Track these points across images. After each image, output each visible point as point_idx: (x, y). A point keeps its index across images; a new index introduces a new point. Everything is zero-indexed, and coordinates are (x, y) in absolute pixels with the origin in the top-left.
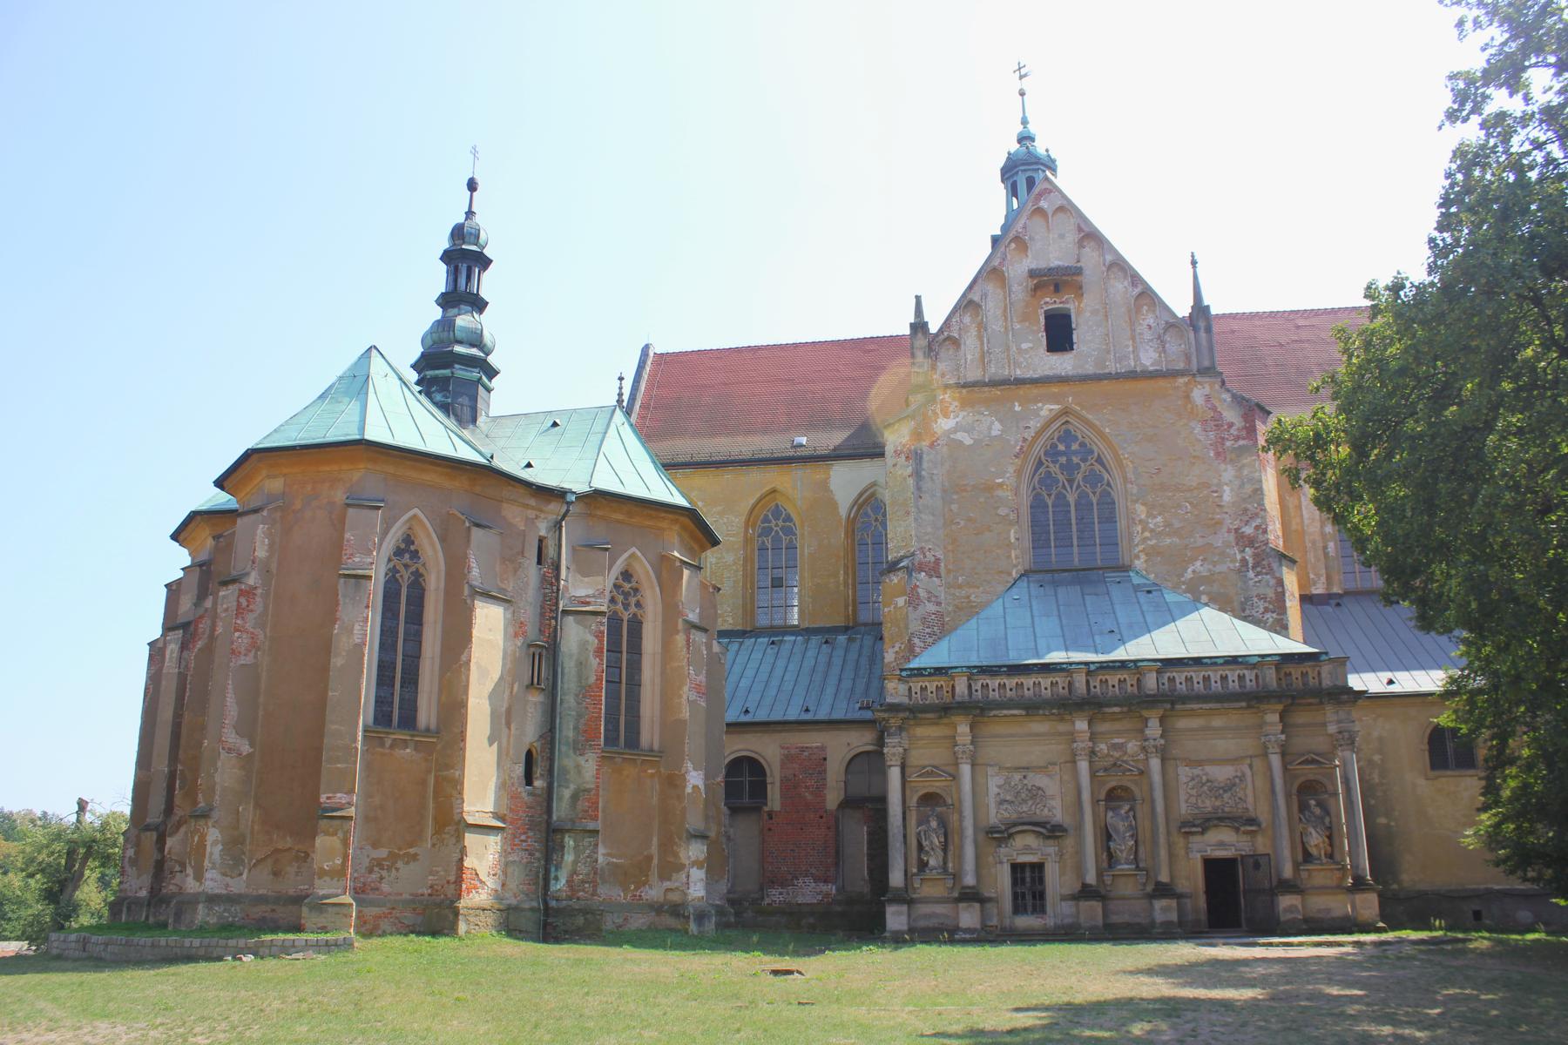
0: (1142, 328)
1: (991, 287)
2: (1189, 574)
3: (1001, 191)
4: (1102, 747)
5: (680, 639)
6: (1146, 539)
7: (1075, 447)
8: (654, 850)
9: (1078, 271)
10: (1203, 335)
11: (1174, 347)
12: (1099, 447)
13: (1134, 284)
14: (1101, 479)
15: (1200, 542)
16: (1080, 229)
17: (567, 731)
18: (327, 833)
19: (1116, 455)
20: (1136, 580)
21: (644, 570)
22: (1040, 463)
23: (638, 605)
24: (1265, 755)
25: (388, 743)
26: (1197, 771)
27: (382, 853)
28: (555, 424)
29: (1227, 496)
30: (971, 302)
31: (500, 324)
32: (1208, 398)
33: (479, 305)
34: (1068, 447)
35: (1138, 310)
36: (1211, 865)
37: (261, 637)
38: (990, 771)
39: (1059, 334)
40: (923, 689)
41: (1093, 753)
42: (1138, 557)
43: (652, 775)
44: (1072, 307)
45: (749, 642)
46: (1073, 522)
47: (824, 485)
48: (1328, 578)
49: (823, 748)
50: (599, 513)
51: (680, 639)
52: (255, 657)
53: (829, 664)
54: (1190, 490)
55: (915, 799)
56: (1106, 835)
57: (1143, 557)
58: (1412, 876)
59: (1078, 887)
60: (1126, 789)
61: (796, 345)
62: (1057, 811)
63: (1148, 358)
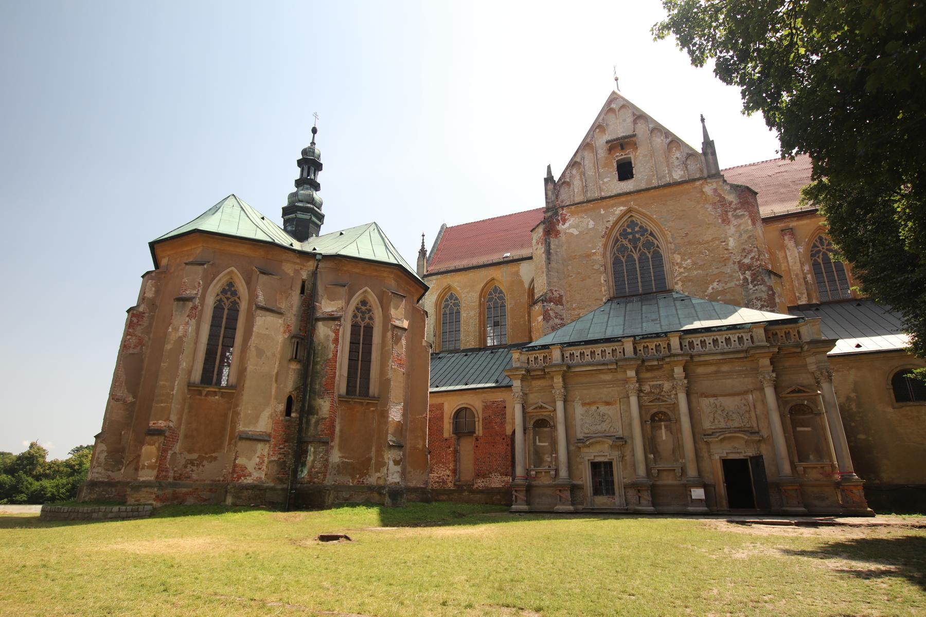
1: (588, 155)
2: (710, 290)
5: (389, 334)
6: (681, 273)
7: (637, 229)
8: (373, 454)
11: (693, 166)
12: (651, 227)
13: (666, 137)
15: (716, 271)
18: (149, 444)
19: (661, 230)
20: (675, 295)
21: (373, 299)
22: (617, 240)
23: (371, 318)
24: (761, 389)
25: (204, 393)
27: (195, 456)
29: (732, 243)
30: (576, 162)
31: (330, 194)
32: (715, 190)
33: (317, 187)
34: (633, 229)
36: (727, 464)
37: (147, 339)
39: (625, 171)
41: (640, 391)
42: (676, 283)
44: (632, 156)
47: (517, 274)
48: (809, 295)
49: (504, 401)
51: (389, 334)
52: (141, 349)
54: (707, 242)
57: (680, 283)
58: (889, 474)
60: (664, 414)
63: (678, 175)
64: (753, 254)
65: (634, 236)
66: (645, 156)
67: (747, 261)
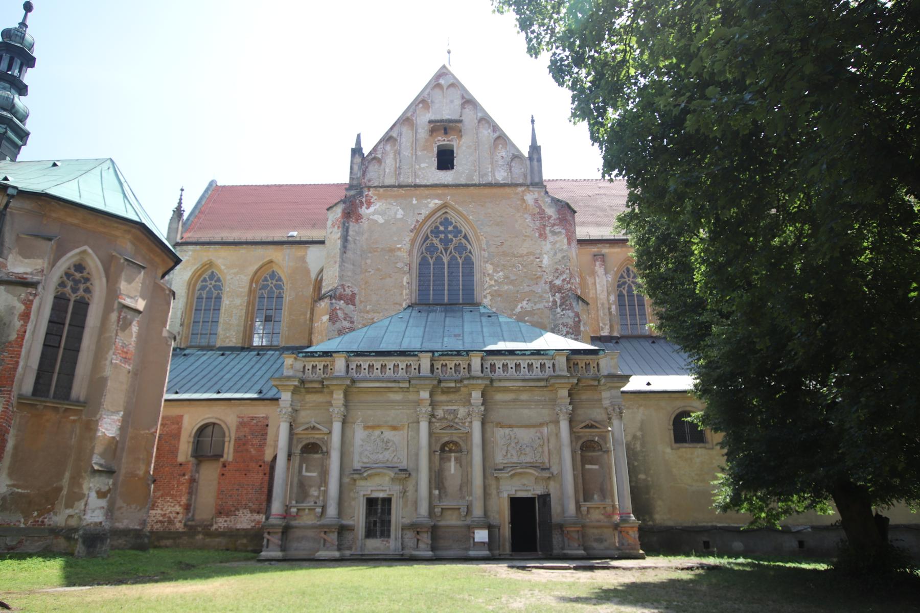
1: (405, 130)
2: (518, 309)
4: (440, 413)
5: (114, 316)
6: (491, 286)
7: (450, 228)
12: (465, 228)
13: (494, 131)
14: (466, 248)
15: (527, 289)
16: (463, 97)
19: (476, 233)
20: (482, 310)
21: (94, 264)
22: (427, 238)
23: (87, 290)
24: (557, 422)
28: (55, 165)
29: (546, 261)
32: (536, 201)
34: (446, 228)
39: (445, 160)
42: (485, 297)
43: (74, 421)
44: (455, 143)
45: (243, 354)
46: (446, 274)
47: (303, 259)
48: (611, 326)
49: (266, 418)
50: (54, 215)
51: (114, 316)
54: (522, 256)
55: (300, 447)
58: (662, 516)
61: (303, 185)
63: (501, 176)
64: (564, 276)
65: (446, 236)
67: (558, 282)
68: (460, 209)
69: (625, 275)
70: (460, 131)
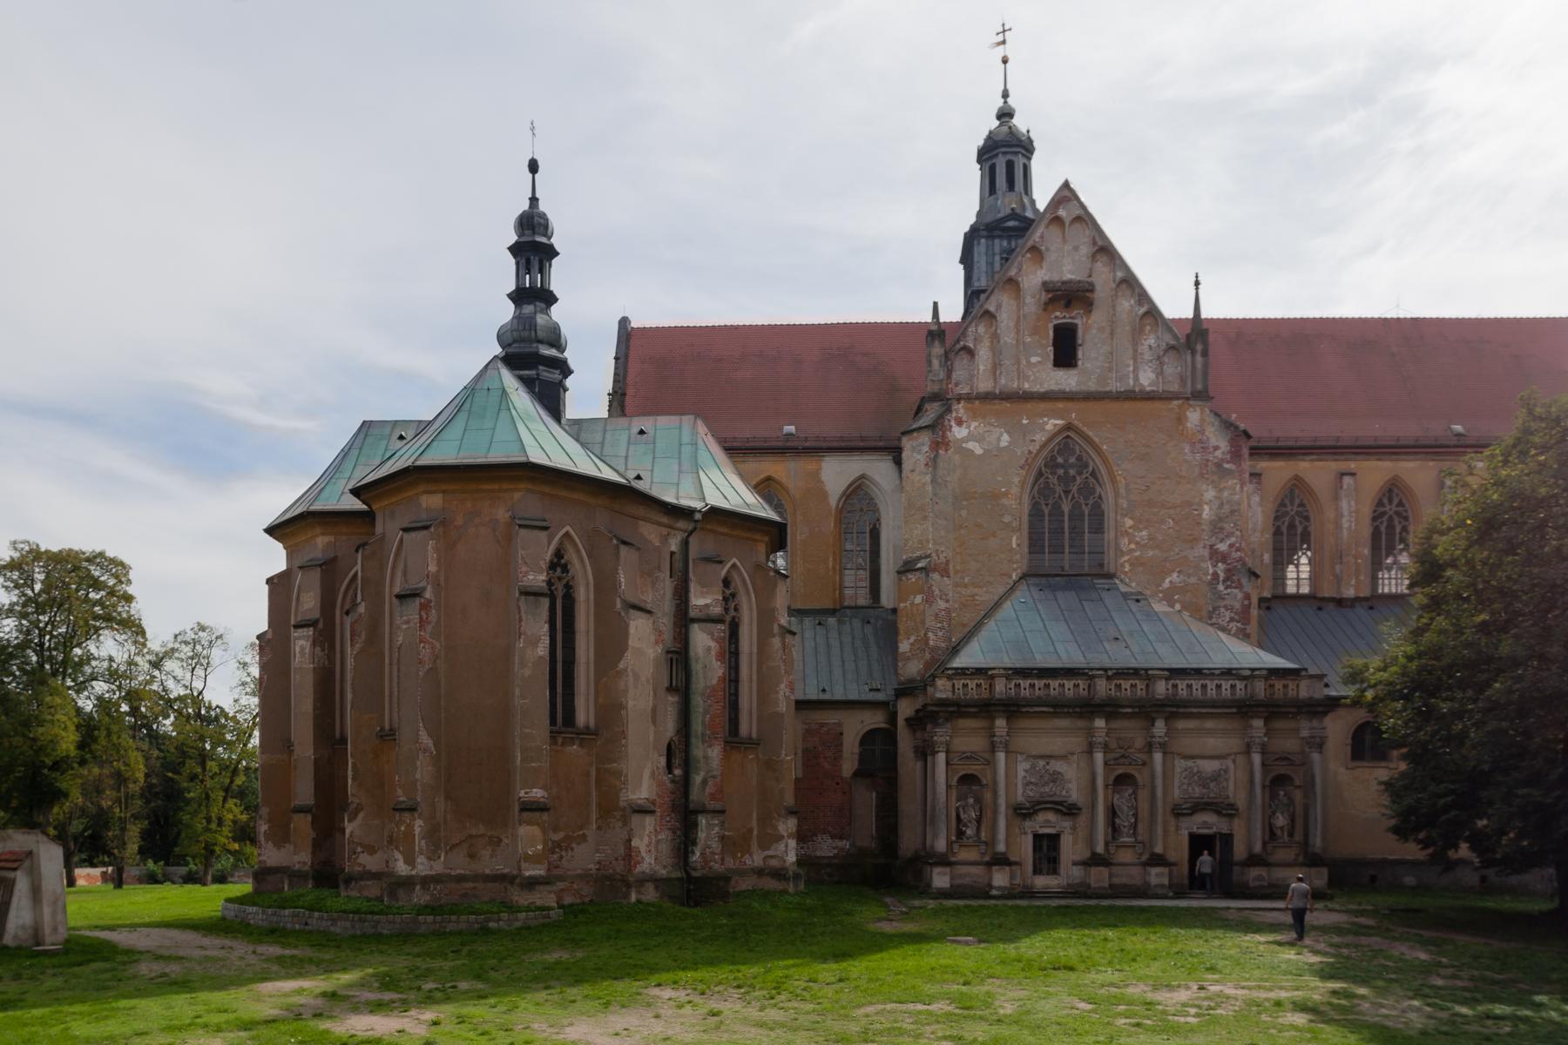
0: (1143, 348)
2: (1166, 584)
3: (973, 175)
5: (776, 642)
6: (1132, 551)
8: (754, 823)
9: (1091, 288)
10: (1199, 359)
13: (1140, 303)
14: (1092, 491)
16: (1095, 243)
17: (697, 726)
20: (1123, 589)
26: (1190, 763)
29: (1206, 512)
35: (1141, 331)
38: (1020, 758)
39: (1065, 350)
40: (965, 686)
47: (815, 476)
49: (839, 724)
53: (828, 645)
56: (1112, 813)
59: (1087, 854)
62: (1074, 792)
64: (1233, 539)
65: (1066, 473)
66: (1101, 329)
67: (1223, 547)
68: (1090, 434)
69: (1385, 501)
70: (1091, 304)
